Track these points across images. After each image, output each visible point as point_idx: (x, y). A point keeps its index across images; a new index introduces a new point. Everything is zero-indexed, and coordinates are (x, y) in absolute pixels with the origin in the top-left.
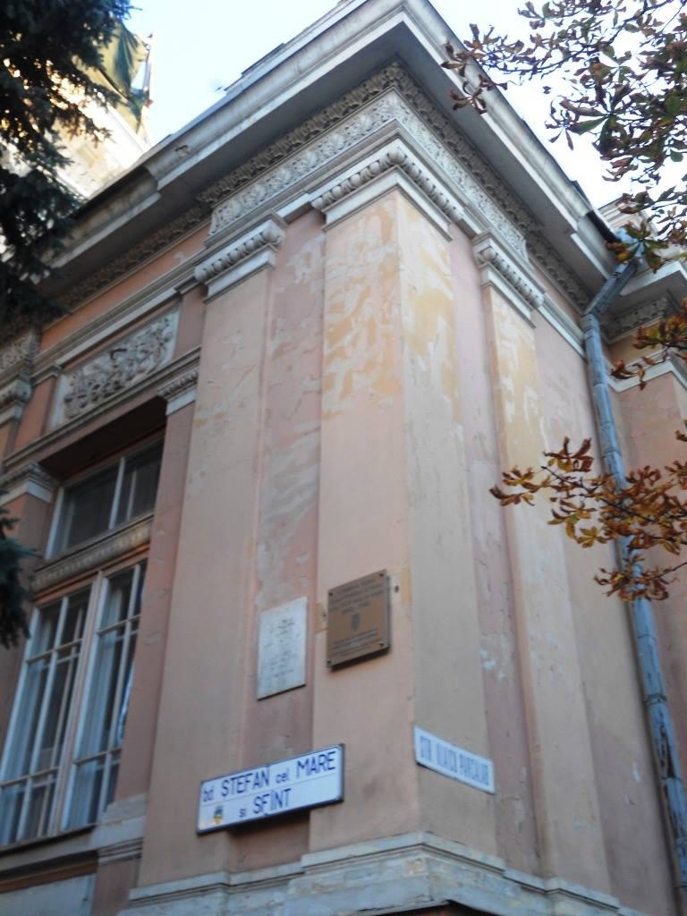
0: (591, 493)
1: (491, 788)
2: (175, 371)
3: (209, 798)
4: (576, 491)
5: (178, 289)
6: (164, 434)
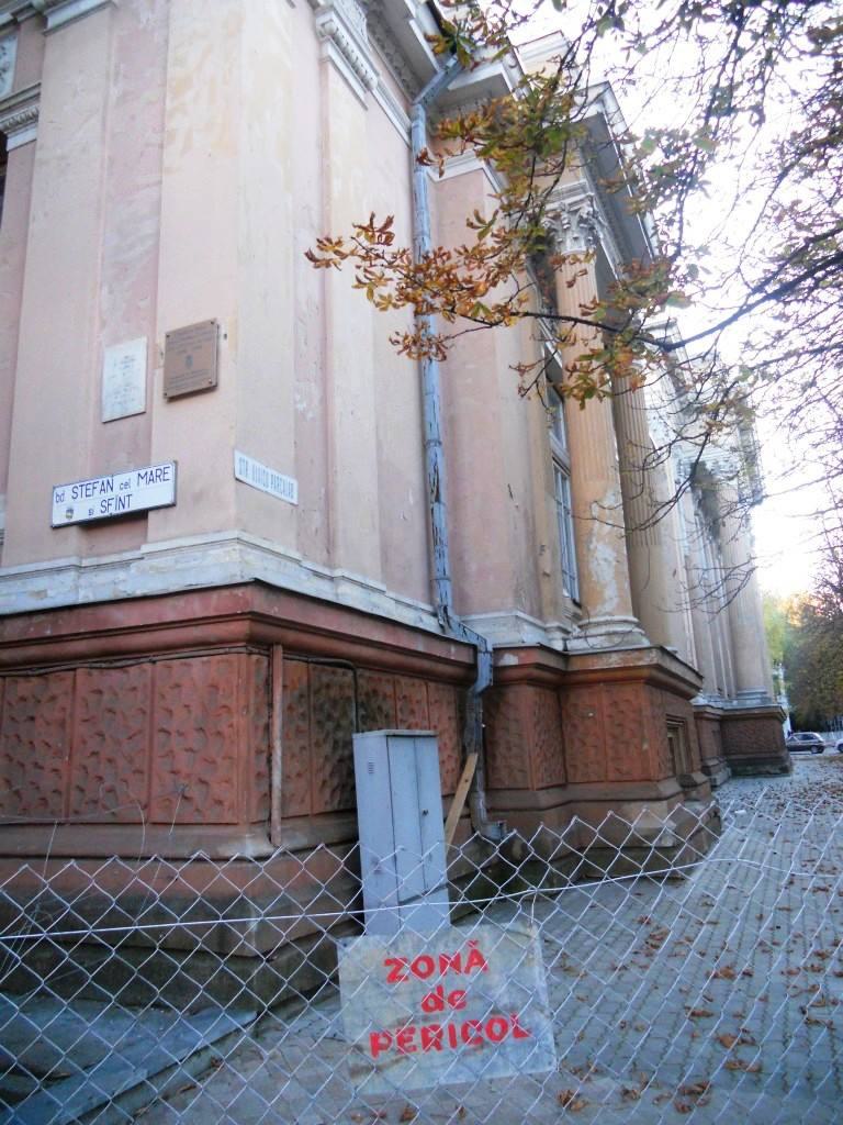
0: (390, 265)
1: (295, 501)
2: (14, 105)
3: (61, 498)
4: (380, 261)
5: (15, 14)
6: (5, 170)
